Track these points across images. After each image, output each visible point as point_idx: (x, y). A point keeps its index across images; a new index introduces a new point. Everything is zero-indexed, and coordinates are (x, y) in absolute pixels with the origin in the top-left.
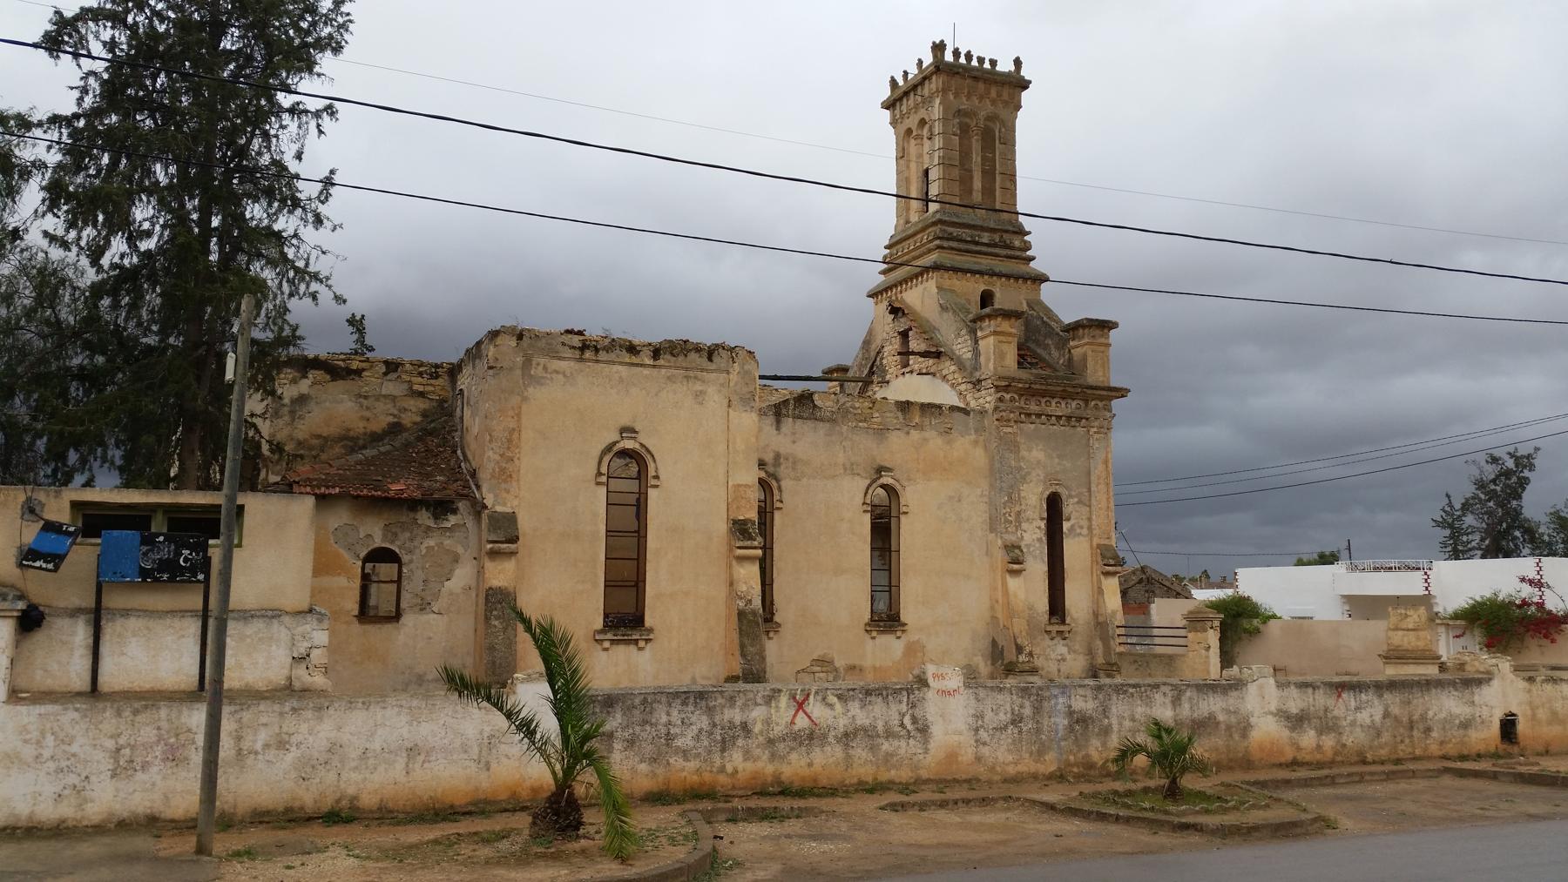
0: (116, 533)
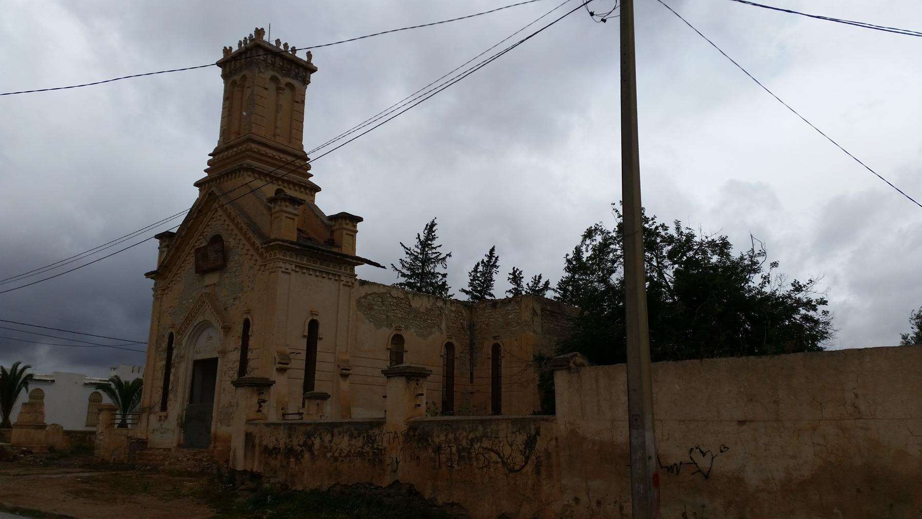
0: (173, 358)
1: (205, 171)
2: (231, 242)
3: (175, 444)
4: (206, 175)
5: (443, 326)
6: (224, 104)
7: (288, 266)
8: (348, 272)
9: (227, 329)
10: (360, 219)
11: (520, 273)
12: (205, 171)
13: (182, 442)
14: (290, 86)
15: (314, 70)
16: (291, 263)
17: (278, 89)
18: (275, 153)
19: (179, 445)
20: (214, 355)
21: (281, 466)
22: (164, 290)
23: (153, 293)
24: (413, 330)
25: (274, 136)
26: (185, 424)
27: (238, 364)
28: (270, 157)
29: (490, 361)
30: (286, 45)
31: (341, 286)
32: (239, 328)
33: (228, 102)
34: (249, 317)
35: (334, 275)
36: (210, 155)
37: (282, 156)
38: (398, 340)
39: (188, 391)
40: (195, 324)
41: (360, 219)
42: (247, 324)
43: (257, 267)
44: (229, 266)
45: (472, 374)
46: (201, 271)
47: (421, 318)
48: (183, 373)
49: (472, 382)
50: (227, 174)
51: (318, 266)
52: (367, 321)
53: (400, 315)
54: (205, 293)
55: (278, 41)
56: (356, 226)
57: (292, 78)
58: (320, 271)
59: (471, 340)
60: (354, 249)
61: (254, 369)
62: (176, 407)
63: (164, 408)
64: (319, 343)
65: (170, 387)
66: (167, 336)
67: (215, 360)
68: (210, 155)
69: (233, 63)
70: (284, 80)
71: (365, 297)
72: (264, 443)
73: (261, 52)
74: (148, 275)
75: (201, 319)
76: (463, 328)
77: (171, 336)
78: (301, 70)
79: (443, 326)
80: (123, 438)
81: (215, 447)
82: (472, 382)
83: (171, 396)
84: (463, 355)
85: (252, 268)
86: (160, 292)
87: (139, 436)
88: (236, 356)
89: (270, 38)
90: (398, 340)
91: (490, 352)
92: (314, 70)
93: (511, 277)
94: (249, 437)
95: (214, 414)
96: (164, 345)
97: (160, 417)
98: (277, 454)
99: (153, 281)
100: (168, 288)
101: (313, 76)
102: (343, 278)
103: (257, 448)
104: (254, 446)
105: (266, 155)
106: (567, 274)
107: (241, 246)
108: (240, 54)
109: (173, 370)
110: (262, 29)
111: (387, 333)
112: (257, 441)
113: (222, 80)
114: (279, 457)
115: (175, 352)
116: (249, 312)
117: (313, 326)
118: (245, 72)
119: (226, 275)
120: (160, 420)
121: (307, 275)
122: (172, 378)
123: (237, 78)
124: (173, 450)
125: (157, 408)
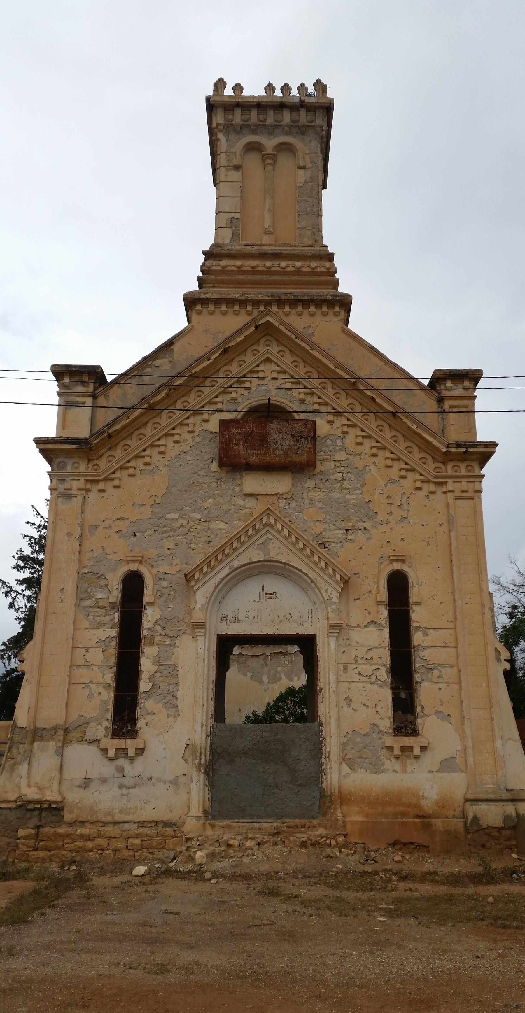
27: (385, 654)
40: (236, 564)
44: (320, 467)
65: (144, 686)
75: (256, 555)
83: (149, 707)
108: (259, 105)
119: (310, 483)
122: (146, 665)
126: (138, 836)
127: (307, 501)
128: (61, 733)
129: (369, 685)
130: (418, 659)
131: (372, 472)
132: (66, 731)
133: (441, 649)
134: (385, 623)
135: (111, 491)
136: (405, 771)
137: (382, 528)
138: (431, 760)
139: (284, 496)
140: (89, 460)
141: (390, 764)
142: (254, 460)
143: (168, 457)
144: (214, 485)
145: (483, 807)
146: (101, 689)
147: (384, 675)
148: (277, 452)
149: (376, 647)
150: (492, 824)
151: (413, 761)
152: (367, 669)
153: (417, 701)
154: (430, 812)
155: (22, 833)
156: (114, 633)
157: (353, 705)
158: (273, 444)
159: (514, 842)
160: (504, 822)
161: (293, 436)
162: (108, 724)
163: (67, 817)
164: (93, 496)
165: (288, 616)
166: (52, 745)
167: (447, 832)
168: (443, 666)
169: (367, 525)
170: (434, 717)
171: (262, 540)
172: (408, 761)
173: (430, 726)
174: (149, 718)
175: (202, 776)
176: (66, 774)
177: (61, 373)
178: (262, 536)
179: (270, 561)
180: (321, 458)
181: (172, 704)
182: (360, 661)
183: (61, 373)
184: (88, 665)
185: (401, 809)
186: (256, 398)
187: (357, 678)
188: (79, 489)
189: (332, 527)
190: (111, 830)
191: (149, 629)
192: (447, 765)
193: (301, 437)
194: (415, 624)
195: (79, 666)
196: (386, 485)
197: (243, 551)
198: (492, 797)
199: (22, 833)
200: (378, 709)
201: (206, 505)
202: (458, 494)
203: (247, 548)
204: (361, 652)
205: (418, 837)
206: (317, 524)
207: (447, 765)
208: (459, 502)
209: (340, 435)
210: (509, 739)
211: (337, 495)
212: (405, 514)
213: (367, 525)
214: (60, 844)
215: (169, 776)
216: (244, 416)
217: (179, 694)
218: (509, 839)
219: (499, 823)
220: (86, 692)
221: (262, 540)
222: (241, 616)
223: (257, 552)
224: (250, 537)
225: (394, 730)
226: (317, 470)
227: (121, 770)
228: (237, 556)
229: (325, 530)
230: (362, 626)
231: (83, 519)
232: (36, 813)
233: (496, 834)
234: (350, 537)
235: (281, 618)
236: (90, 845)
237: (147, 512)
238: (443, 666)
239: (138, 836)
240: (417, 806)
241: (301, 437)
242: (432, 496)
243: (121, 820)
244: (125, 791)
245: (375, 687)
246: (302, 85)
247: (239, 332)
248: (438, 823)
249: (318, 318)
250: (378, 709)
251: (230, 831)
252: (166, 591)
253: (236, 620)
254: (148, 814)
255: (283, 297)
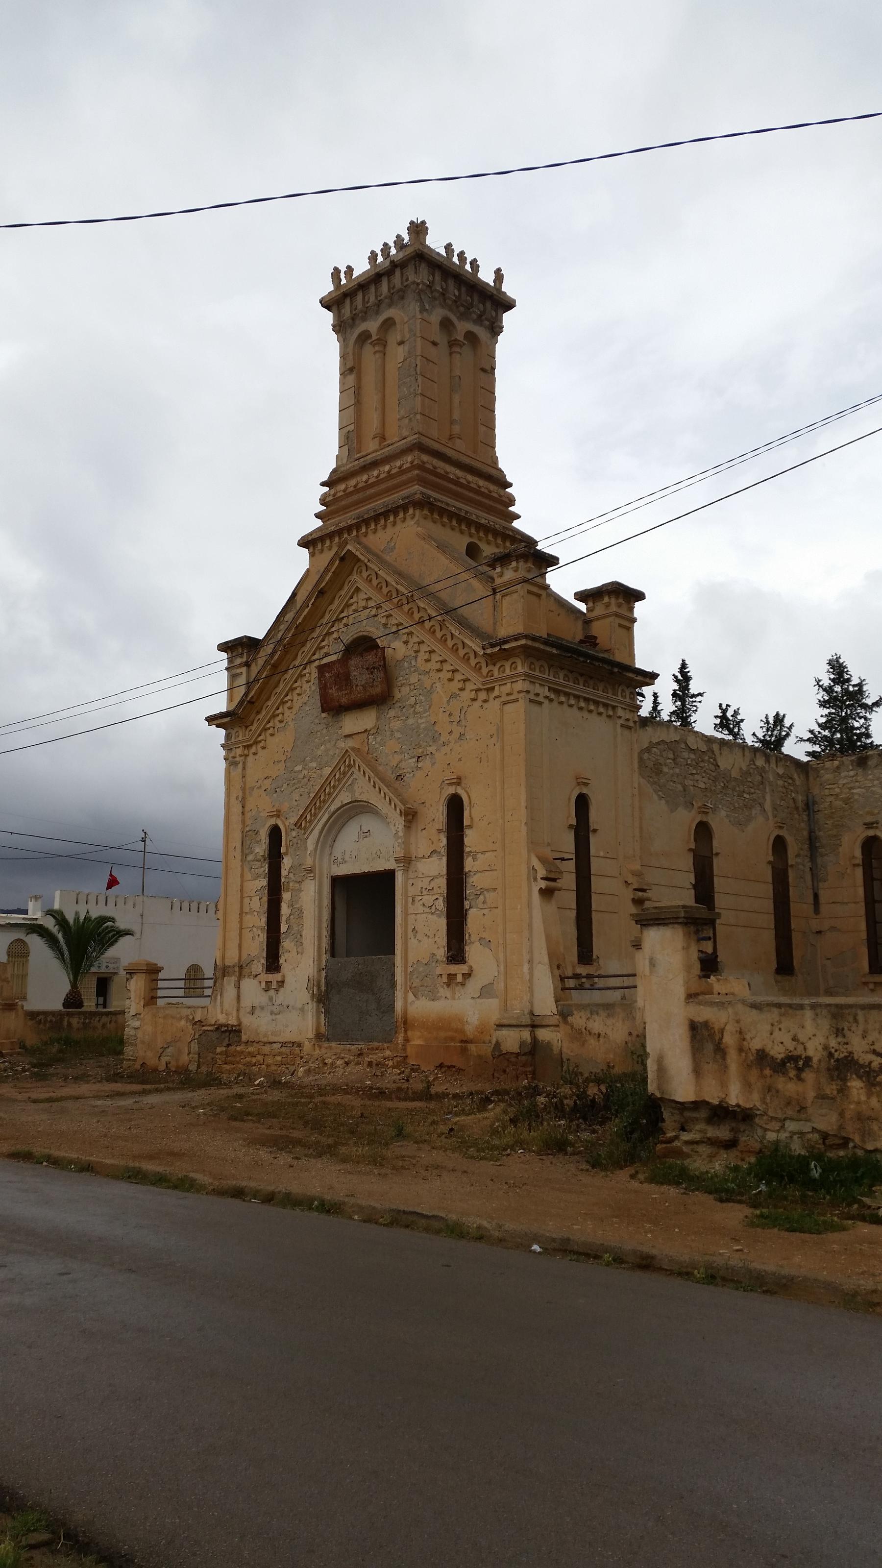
0: (284, 872)
1: (318, 516)
2: (397, 649)
3: (311, 1034)
4: (319, 523)
5: (768, 806)
6: (342, 383)
7: (538, 689)
8: (628, 700)
9: (410, 816)
10: (639, 596)
11: (736, 713)
12: (318, 516)
13: (323, 1030)
14: (472, 338)
15: (508, 305)
16: (543, 682)
17: (452, 344)
18: (459, 473)
19: (319, 1036)
20: (390, 865)
21: (821, 1097)
22: (248, 747)
23: (223, 753)
24: (723, 813)
25: (451, 438)
26: (325, 995)
27: (442, 882)
28: (450, 481)
29: (859, 872)
30: (461, 255)
31: (619, 729)
32: (438, 814)
33: (351, 379)
34: (460, 791)
35: (606, 705)
36: (323, 484)
37: (470, 477)
38: (703, 831)
39: (325, 933)
40: (333, 808)
41: (639, 596)
42: (455, 806)
43: (467, 695)
44: (397, 695)
45: (816, 896)
46: (333, 709)
47: (734, 790)
48: (308, 905)
49: (817, 910)
50: (376, 518)
51: (580, 689)
52: (655, 797)
53: (702, 785)
54: (353, 749)
55: (449, 247)
56: (631, 609)
57: (475, 322)
58: (587, 700)
59: (811, 832)
60: (632, 655)
61: (482, 891)
62: (303, 962)
63: (273, 962)
64: (593, 840)
65: (284, 928)
66: (264, 835)
67: (390, 875)
68: (323, 484)
69: (360, 296)
70: (463, 327)
71: (648, 750)
72: (756, 1045)
73: (424, 269)
74: (211, 720)
75: (344, 797)
76: (797, 808)
77: (275, 834)
78: (488, 305)
79: (768, 806)
80: (183, 1022)
81: (407, 1040)
82: (817, 910)
83: (287, 944)
84: (799, 860)
85: (453, 696)
86: (236, 755)
87: (222, 1019)
88: (438, 866)
89: (435, 242)
90: (703, 831)
91: (858, 853)
92: (508, 305)
93: (718, 721)
94: (699, 1033)
95: (399, 977)
96: (261, 848)
97: (268, 983)
98: (800, 1070)
99: (222, 732)
100: (256, 742)
101: (508, 318)
102: (620, 712)
103: (733, 1060)
104: (720, 1050)
105: (445, 477)
106: (826, 711)
107: (422, 656)
108: (375, 278)
109: (286, 896)
110: (423, 223)
111: (687, 818)
112: (729, 1040)
113: (334, 336)
114: (809, 1076)
115: (287, 863)
116: (458, 782)
117: (582, 803)
118: (391, 312)
119: (392, 713)
120: (266, 990)
121: (565, 706)
122: (285, 910)
123: (372, 326)
124: (307, 1046)
125: (259, 966)
126: (280, 1054)
127: (388, 733)
128: (237, 969)
129: (430, 916)
130: (468, 886)
131: (438, 690)
132: (241, 967)
133: (487, 873)
134: (444, 851)
135: (260, 751)
136: (454, 999)
137: (444, 750)
138: (474, 986)
139: (372, 732)
140: (247, 727)
141: (444, 992)
142: (344, 700)
143: (294, 711)
144: (325, 731)
145: (505, 1032)
146: (259, 932)
147: (441, 905)
148: (358, 688)
149: (436, 877)
150: (511, 1050)
151: (460, 987)
152: (428, 899)
153: (466, 928)
154: (472, 1037)
155: (219, 1050)
156: (265, 882)
157: (419, 936)
158: (354, 681)
159: (530, 1069)
160: (520, 1048)
161: (367, 669)
162: (263, 961)
163: (244, 1038)
164: (251, 758)
165: (379, 853)
166: (234, 979)
167: (480, 1057)
168: (488, 890)
169: (432, 749)
170: (478, 944)
171: (349, 783)
172: (457, 988)
173: (474, 952)
174: (287, 955)
175: (315, 1004)
176: (242, 1004)
177: (224, 647)
178: (349, 778)
179: (356, 801)
180: (399, 684)
181: (299, 943)
182: (425, 892)
183: (224, 647)
184: (252, 911)
185: (450, 1034)
186: (348, 636)
187: (421, 909)
188: (240, 756)
189: (407, 756)
190: (266, 1049)
191: (286, 877)
192: (486, 991)
193: (374, 668)
194: (467, 849)
195: (246, 913)
196: (448, 701)
197: (337, 795)
198: (514, 1022)
199: (219, 1050)
200: (436, 939)
201: (319, 753)
202: (504, 698)
203: (340, 791)
204: (425, 883)
205: (457, 1061)
206: (396, 755)
207: (486, 991)
208: (507, 707)
209: (414, 654)
210: (540, 963)
211: (411, 721)
212: (462, 730)
213: (432, 749)
214: (238, 1059)
215: (299, 1006)
216: (343, 656)
217: (304, 934)
218: (524, 1065)
219: (515, 1049)
220: (251, 935)
221: (349, 783)
222: (347, 858)
223: (347, 794)
224: (339, 780)
225: (448, 958)
226: (396, 699)
227: (271, 999)
228: (333, 801)
229: (401, 761)
230: (427, 856)
231: (245, 783)
232: (227, 1034)
233: (513, 1059)
234: (420, 765)
235: (374, 856)
236: (254, 1060)
237: (282, 766)
238: (488, 890)
239: (280, 1054)
240: (463, 1032)
241: (374, 668)
242: (485, 705)
243: (272, 1040)
244: (274, 1017)
245: (435, 917)
246: (398, 236)
247: (327, 570)
248: (472, 1048)
249: (390, 530)
250: (436, 939)
251: (332, 1051)
252: (295, 840)
253: (344, 861)
254: (287, 1037)
255: (366, 516)
